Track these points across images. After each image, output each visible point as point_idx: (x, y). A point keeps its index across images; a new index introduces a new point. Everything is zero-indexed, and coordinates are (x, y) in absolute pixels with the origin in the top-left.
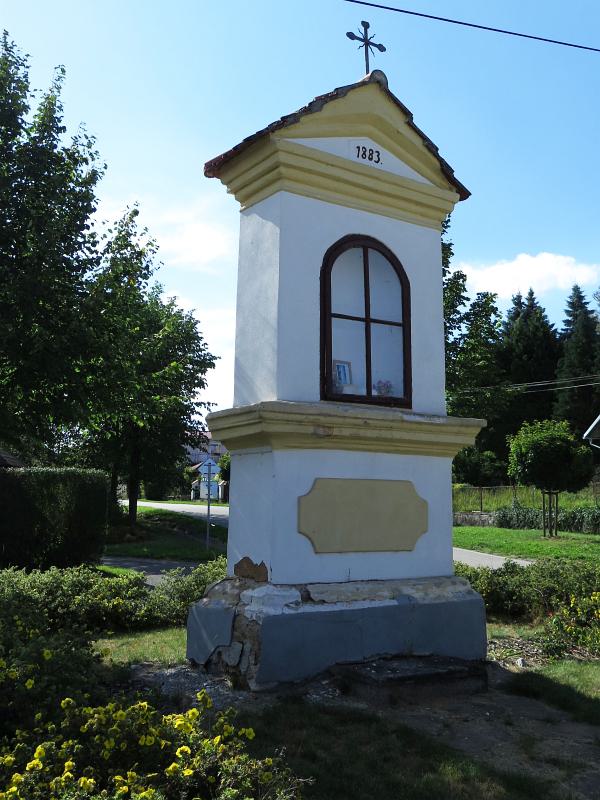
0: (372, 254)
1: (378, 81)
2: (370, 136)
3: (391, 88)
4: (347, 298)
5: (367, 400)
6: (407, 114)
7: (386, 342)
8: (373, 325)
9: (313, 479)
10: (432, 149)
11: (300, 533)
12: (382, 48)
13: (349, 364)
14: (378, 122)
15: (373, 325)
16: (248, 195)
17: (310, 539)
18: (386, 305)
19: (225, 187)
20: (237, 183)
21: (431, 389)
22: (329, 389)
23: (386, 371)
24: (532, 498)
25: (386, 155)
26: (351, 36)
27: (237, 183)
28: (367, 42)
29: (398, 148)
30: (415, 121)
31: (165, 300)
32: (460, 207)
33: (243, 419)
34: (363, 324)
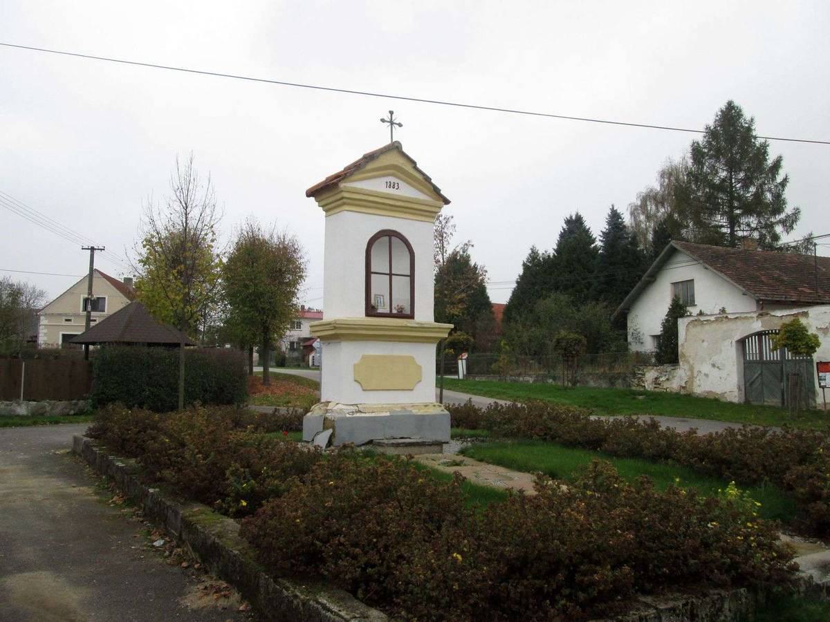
0: (394, 239)
1: (395, 147)
2: (392, 175)
3: (405, 150)
4: (379, 264)
5: (390, 315)
6: (413, 163)
7: (401, 284)
8: (388, 272)
9: (363, 392)
10: (428, 179)
11: (355, 381)
12: (400, 125)
13: (383, 296)
14: (395, 167)
15: (388, 272)
16: (328, 209)
17: (359, 383)
18: (401, 266)
19: (317, 203)
20: (323, 203)
21: (425, 312)
22: (371, 310)
23: (401, 298)
24: (492, 375)
25: (402, 184)
26: (383, 120)
27: (323, 203)
28: (392, 123)
29: (409, 180)
30: (418, 166)
31: (662, 329)
32: (445, 207)
33: (327, 327)
34: (388, 276)
